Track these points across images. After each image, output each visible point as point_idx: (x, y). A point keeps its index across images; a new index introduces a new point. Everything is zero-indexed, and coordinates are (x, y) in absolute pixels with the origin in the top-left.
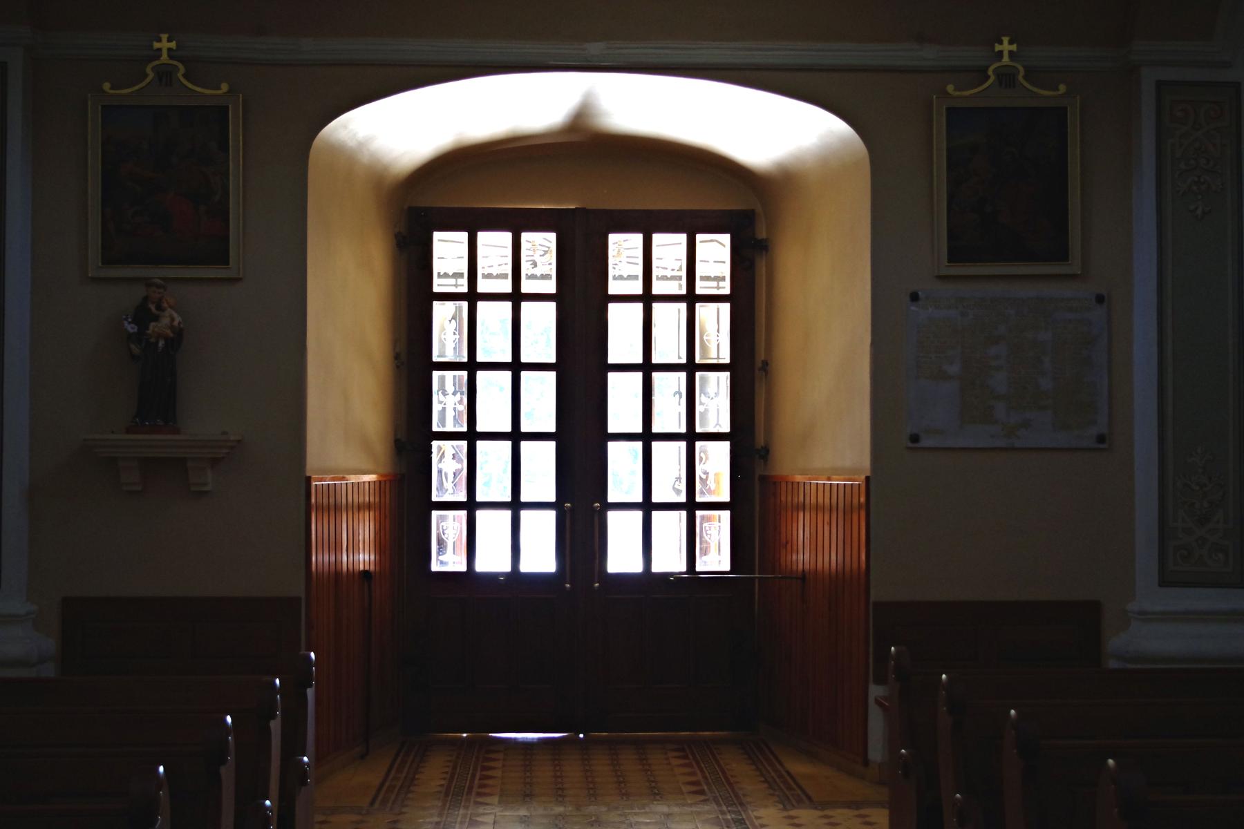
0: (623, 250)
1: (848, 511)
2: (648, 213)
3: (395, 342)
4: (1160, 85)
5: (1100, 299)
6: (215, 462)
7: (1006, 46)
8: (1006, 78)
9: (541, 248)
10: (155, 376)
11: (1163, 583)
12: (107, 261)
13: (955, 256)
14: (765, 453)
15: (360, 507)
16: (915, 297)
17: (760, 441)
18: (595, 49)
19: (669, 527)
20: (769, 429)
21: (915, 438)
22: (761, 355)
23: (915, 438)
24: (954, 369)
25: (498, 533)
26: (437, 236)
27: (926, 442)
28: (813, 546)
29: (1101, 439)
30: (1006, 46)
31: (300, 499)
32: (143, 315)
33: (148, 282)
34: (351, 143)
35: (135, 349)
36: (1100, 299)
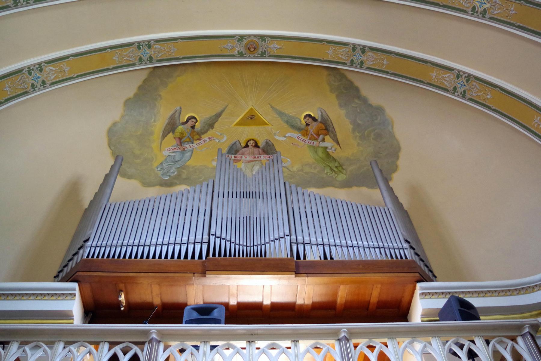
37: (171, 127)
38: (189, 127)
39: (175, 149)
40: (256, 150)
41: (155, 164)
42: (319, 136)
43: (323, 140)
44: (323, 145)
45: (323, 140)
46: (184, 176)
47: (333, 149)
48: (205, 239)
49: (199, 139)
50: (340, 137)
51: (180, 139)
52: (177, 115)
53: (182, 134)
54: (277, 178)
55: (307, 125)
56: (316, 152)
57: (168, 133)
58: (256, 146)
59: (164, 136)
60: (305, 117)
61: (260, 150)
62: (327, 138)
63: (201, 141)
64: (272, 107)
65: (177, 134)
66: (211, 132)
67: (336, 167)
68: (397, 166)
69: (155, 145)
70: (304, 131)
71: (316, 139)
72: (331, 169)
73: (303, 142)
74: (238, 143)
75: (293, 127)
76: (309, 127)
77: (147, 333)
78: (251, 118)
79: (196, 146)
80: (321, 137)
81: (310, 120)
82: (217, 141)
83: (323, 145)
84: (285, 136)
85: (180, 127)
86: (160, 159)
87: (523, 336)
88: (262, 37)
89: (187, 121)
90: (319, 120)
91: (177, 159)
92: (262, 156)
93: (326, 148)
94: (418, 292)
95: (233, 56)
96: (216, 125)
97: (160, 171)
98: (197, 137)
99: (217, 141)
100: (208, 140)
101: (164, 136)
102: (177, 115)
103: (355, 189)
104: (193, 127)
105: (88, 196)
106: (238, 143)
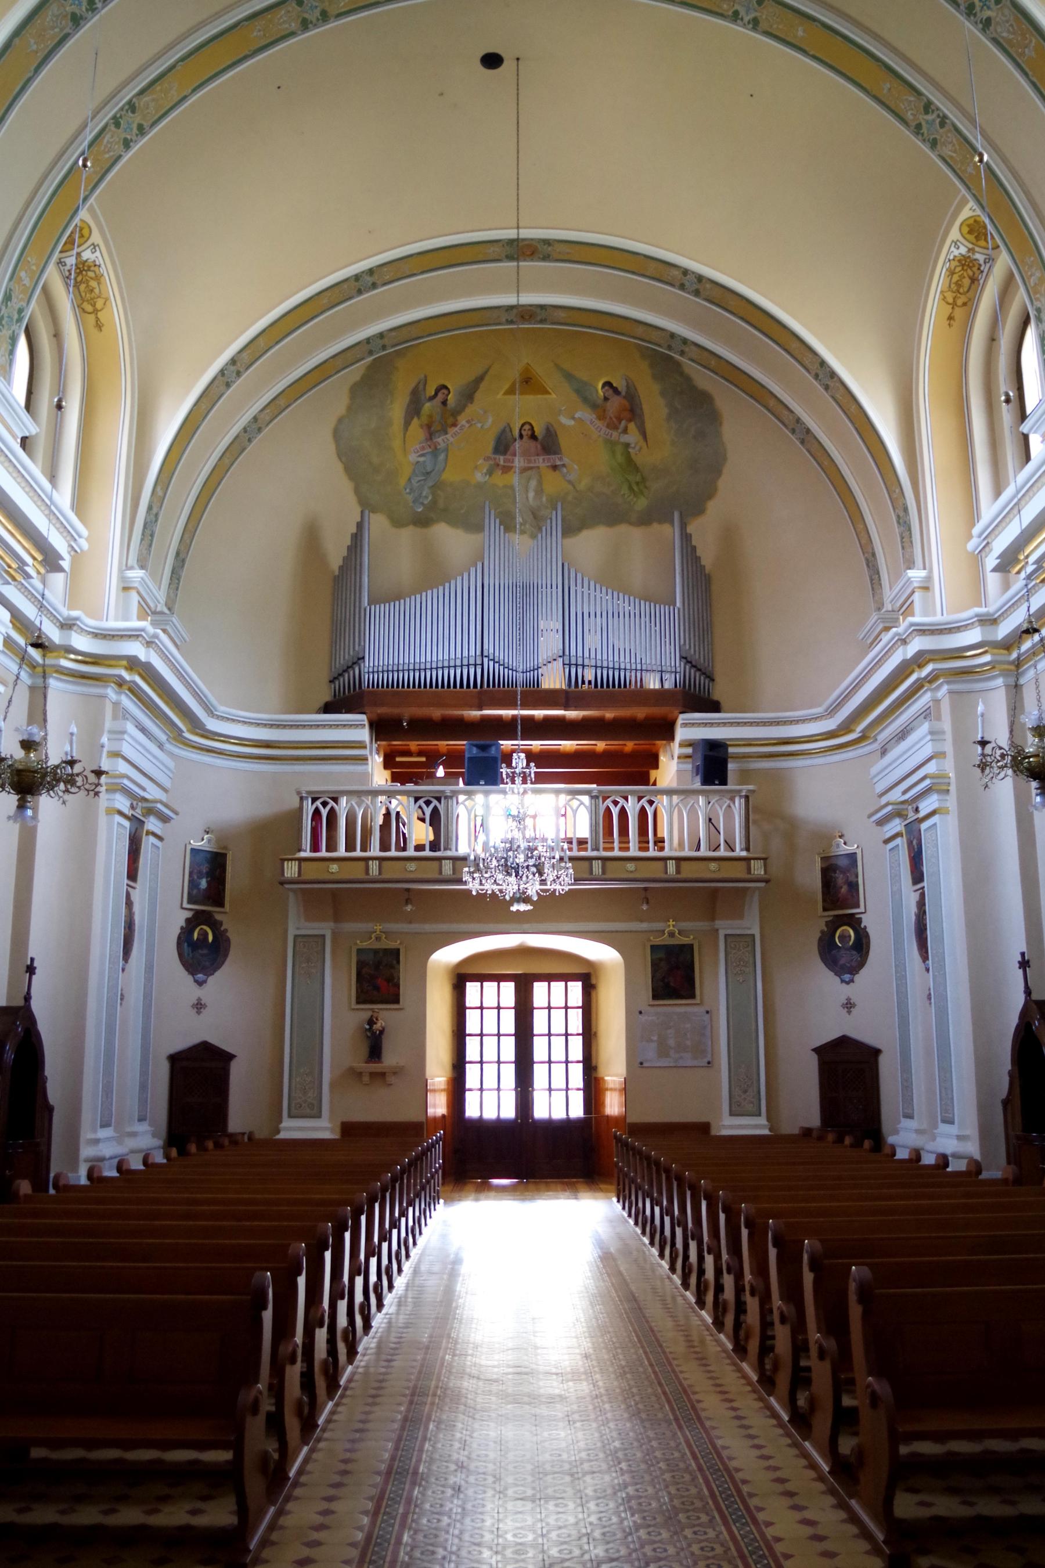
0: (539, 989)
1: (620, 1091)
2: (549, 974)
3: (453, 1026)
4: (726, 936)
5: (707, 1012)
6: (395, 1073)
7: (671, 923)
8: (672, 935)
9: (508, 989)
10: (374, 1044)
11: (731, 1115)
12: (358, 1003)
13: (655, 997)
14: (595, 1068)
15: (611, 1089)
16: (640, 1013)
17: (594, 1064)
18: (526, 926)
19: (559, 1097)
20: (597, 1059)
21: (641, 1063)
22: (594, 1030)
23: (641, 1063)
24: (655, 1038)
25: (491, 1101)
26: (468, 984)
27: (645, 1065)
28: (613, 1105)
29: (709, 1063)
30: (671, 923)
31: (424, 1089)
32: (371, 1022)
33: (373, 1010)
34: (565, 1190)
35: (369, 1034)
36: (707, 1012)
37: (414, 409)
38: (440, 404)
39: (423, 448)
40: (532, 444)
41: (402, 482)
42: (620, 420)
43: (625, 431)
44: (625, 439)
45: (625, 431)
46: (441, 504)
47: (637, 448)
48: (479, 662)
49: (454, 425)
50: (649, 426)
51: (429, 426)
52: (421, 387)
53: (430, 416)
54: (554, 560)
55: (606, 399)
56: (613, 453)
57: (412, 418)
58: (533, 437)
59: (407, 424)
60: (603, 387)
61: (539, 446)
62: (632, 426)
63: (456, 429)
64: (557, 365)
65: (424, 419)
66: (471, 410)
67: (637, 483)
68: (716, 490)
69: (397, 444)
70: (598, 408)
71: (616, 428)
72: (630, 488)
73: (597, 429)
74: (508, 430)
75: (586, 400)
76: (609, 404)
77: (443, 792)
78: (528, 383)
79: (451, 439)
80: (623, 423)
81: (611, 391)
82: (479, 425)
83: (625, 439)
84: (573, 418)
85: (428, 405)
86: (407, 472)
87: (741, 797)
88: (542, 307)
89: (436, 394)
90: (623, 393)
91: (429, 469)
92: (541, 458)
93: (627, 445)
94: (680, 721)
95: (499, 324)
96: (478, 395)
97: (410, 493)
98: (450, 420)
99: (479, 425)
100: (467, 425)
101: (407, 424)
102: (421, 387)
103: (656, 526)
104: (444, 403)
105: (335, 553)
106: (508, 430)
